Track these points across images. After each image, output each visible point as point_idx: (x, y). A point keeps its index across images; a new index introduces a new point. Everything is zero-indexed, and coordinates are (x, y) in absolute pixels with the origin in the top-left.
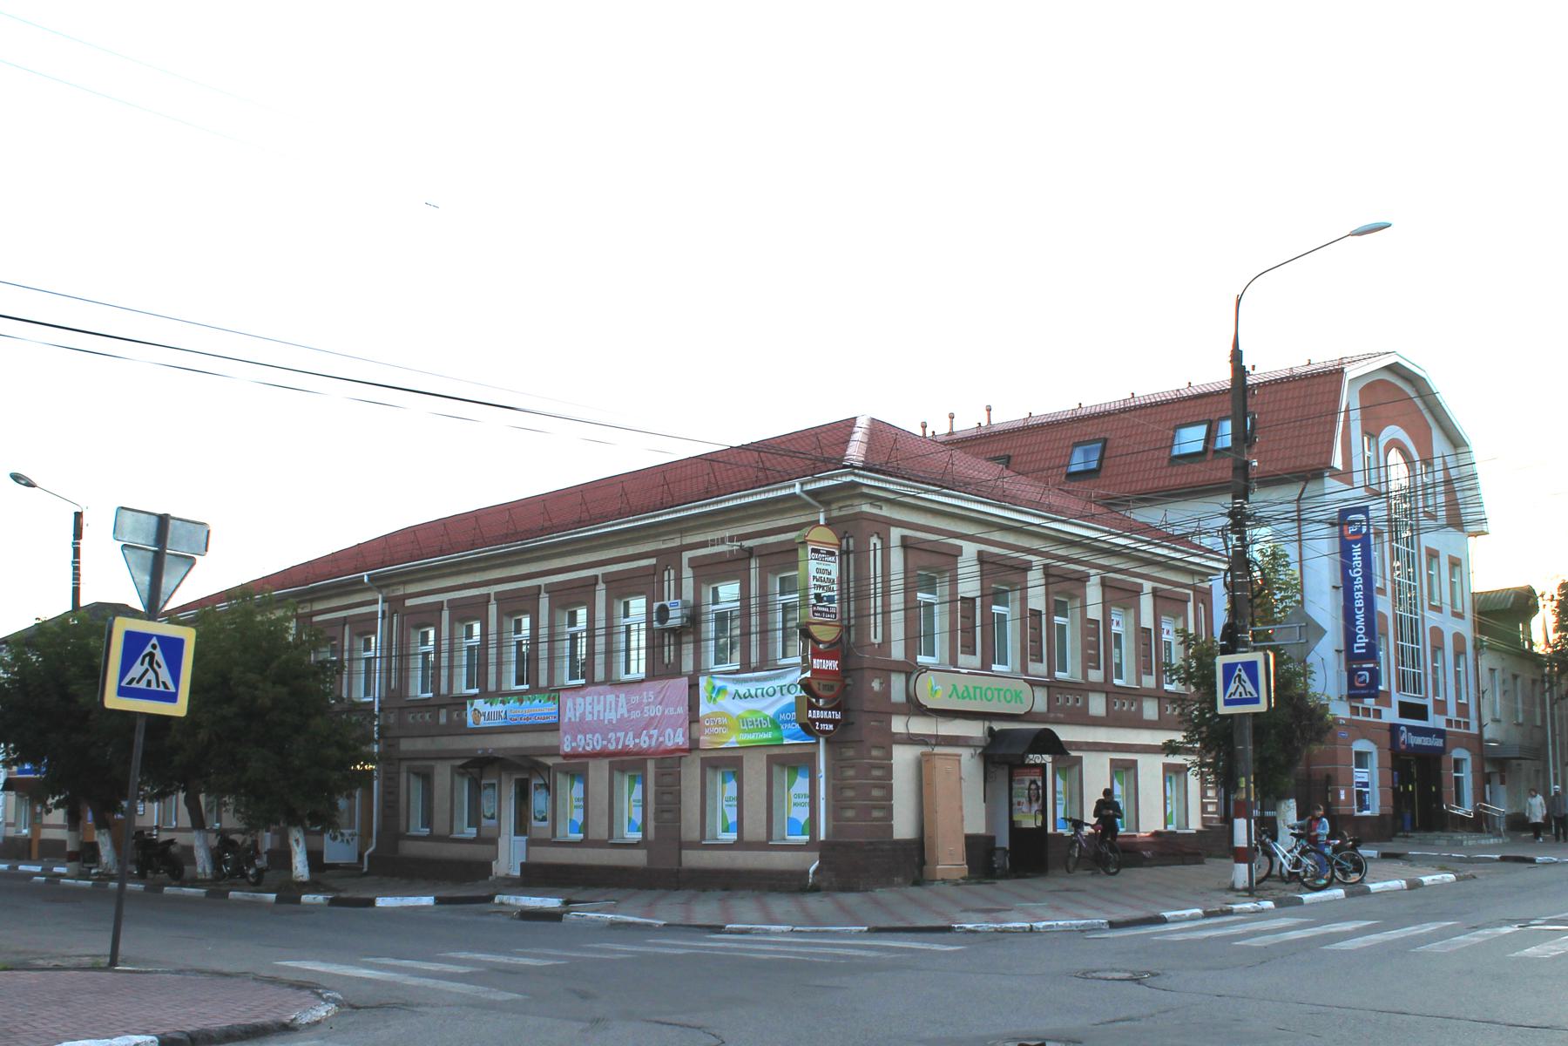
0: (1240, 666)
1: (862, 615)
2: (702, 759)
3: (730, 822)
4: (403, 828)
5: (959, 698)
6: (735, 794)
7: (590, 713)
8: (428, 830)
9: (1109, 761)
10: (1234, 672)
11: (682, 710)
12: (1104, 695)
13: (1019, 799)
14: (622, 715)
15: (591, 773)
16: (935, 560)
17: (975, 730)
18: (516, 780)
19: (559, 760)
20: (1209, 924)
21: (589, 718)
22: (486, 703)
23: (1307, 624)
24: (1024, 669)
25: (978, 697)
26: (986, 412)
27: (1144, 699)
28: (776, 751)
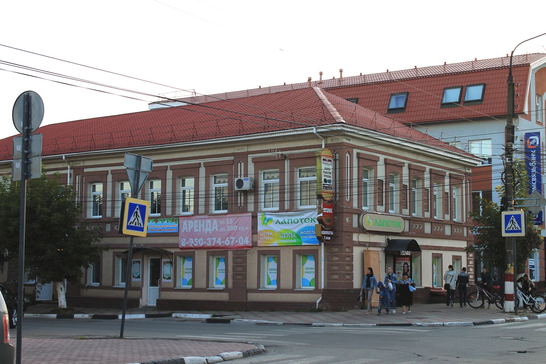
0: (513, 216)
2: (258, 251)
3: (271, 280)
5: (378, 226)
7: (197, 228)
8: (99, 283)
9: (431, 254)
10: (510, 219)
11: (249, 228)
12: (450, 226)
13: (399, 271)
14: (215, 230)
15: (197, 257)
16: (370, 163)
17: (382, 240)
18: (151, 259)
19: (179, 250)
20: (511, 325)
21: (196, 230)
23: (539, 198)
26: (340, 73)
27: (446, 225)
28: (298, 248)
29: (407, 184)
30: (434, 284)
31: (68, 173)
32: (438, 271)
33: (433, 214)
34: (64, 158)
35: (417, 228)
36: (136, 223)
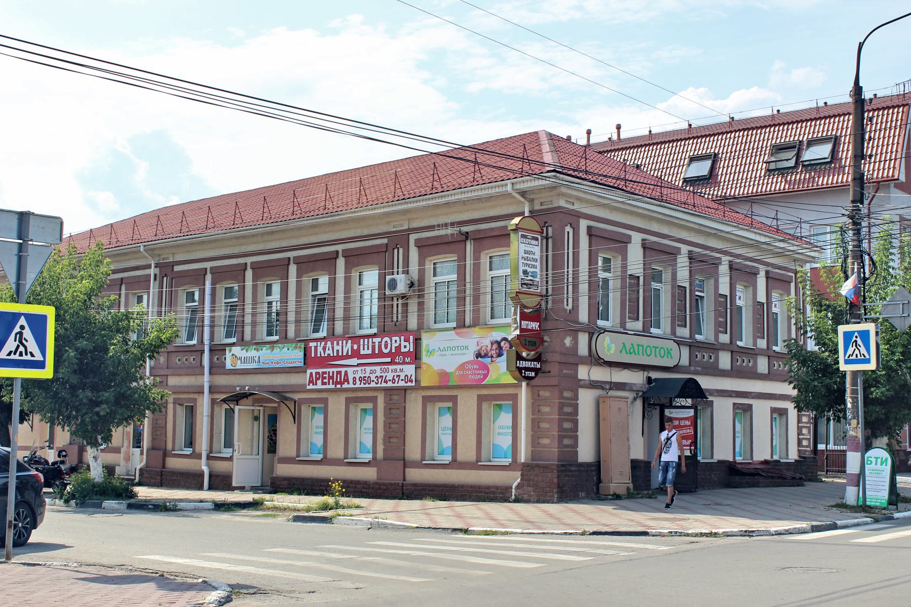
0: (856, 334)
1: (558, 291)
5: (627, 353)
6: (450, 425)
8: (191, 449)
17: (637, 378)
22: (242, 350)
24: (673, 332)
25: (641, 353)
29: (687, 285)
30: (737, 454)
33: (770, 344)
34: (142, 249)
35: (705, 360)
36: (857, 355)
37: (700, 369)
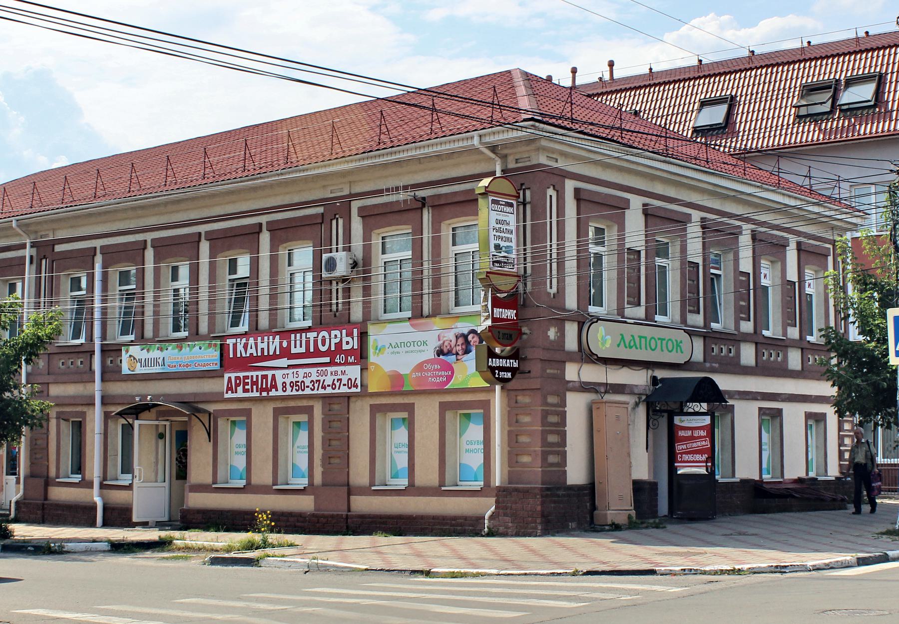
4: (53, 472)
8: (80, 476)
17: (639, 378)
24: (684, 320)
29: (699, 260)
31: (25, 256)
32: (773, 446)
37: (716, 365)
